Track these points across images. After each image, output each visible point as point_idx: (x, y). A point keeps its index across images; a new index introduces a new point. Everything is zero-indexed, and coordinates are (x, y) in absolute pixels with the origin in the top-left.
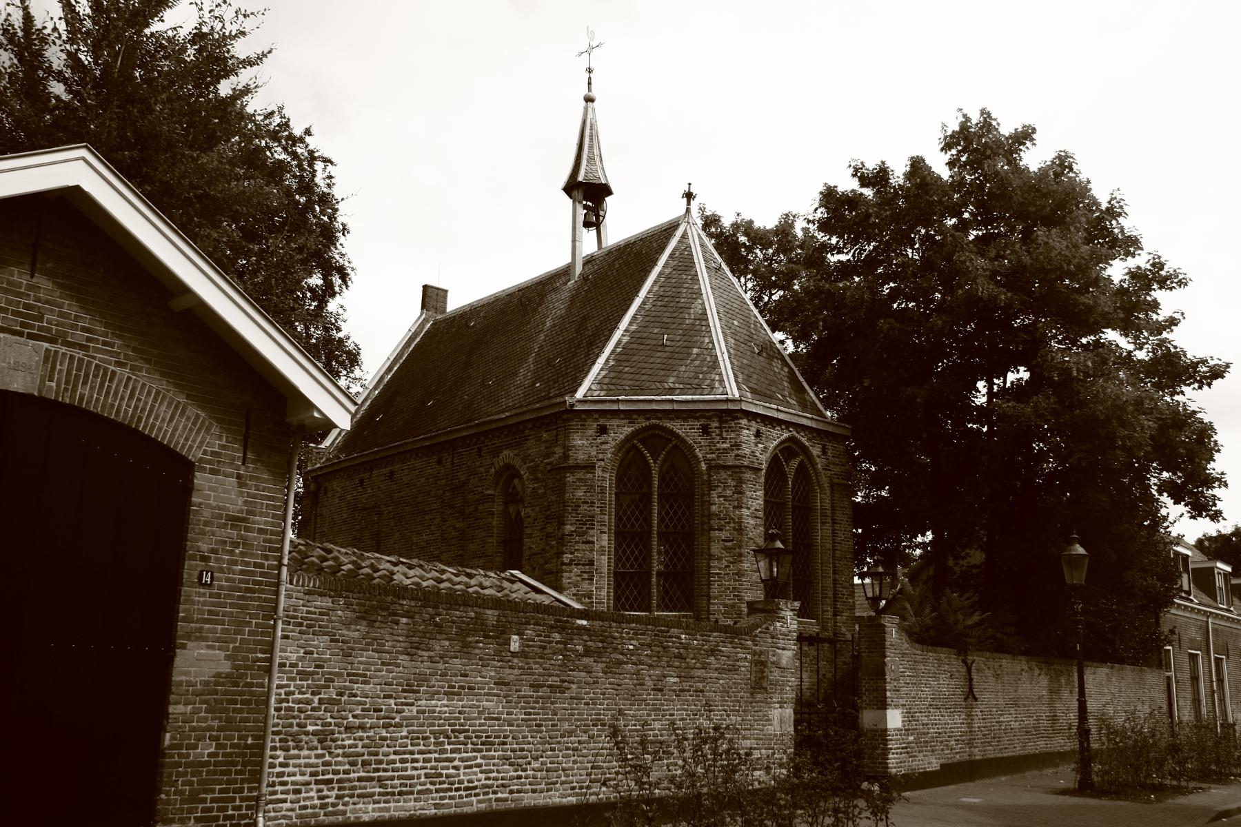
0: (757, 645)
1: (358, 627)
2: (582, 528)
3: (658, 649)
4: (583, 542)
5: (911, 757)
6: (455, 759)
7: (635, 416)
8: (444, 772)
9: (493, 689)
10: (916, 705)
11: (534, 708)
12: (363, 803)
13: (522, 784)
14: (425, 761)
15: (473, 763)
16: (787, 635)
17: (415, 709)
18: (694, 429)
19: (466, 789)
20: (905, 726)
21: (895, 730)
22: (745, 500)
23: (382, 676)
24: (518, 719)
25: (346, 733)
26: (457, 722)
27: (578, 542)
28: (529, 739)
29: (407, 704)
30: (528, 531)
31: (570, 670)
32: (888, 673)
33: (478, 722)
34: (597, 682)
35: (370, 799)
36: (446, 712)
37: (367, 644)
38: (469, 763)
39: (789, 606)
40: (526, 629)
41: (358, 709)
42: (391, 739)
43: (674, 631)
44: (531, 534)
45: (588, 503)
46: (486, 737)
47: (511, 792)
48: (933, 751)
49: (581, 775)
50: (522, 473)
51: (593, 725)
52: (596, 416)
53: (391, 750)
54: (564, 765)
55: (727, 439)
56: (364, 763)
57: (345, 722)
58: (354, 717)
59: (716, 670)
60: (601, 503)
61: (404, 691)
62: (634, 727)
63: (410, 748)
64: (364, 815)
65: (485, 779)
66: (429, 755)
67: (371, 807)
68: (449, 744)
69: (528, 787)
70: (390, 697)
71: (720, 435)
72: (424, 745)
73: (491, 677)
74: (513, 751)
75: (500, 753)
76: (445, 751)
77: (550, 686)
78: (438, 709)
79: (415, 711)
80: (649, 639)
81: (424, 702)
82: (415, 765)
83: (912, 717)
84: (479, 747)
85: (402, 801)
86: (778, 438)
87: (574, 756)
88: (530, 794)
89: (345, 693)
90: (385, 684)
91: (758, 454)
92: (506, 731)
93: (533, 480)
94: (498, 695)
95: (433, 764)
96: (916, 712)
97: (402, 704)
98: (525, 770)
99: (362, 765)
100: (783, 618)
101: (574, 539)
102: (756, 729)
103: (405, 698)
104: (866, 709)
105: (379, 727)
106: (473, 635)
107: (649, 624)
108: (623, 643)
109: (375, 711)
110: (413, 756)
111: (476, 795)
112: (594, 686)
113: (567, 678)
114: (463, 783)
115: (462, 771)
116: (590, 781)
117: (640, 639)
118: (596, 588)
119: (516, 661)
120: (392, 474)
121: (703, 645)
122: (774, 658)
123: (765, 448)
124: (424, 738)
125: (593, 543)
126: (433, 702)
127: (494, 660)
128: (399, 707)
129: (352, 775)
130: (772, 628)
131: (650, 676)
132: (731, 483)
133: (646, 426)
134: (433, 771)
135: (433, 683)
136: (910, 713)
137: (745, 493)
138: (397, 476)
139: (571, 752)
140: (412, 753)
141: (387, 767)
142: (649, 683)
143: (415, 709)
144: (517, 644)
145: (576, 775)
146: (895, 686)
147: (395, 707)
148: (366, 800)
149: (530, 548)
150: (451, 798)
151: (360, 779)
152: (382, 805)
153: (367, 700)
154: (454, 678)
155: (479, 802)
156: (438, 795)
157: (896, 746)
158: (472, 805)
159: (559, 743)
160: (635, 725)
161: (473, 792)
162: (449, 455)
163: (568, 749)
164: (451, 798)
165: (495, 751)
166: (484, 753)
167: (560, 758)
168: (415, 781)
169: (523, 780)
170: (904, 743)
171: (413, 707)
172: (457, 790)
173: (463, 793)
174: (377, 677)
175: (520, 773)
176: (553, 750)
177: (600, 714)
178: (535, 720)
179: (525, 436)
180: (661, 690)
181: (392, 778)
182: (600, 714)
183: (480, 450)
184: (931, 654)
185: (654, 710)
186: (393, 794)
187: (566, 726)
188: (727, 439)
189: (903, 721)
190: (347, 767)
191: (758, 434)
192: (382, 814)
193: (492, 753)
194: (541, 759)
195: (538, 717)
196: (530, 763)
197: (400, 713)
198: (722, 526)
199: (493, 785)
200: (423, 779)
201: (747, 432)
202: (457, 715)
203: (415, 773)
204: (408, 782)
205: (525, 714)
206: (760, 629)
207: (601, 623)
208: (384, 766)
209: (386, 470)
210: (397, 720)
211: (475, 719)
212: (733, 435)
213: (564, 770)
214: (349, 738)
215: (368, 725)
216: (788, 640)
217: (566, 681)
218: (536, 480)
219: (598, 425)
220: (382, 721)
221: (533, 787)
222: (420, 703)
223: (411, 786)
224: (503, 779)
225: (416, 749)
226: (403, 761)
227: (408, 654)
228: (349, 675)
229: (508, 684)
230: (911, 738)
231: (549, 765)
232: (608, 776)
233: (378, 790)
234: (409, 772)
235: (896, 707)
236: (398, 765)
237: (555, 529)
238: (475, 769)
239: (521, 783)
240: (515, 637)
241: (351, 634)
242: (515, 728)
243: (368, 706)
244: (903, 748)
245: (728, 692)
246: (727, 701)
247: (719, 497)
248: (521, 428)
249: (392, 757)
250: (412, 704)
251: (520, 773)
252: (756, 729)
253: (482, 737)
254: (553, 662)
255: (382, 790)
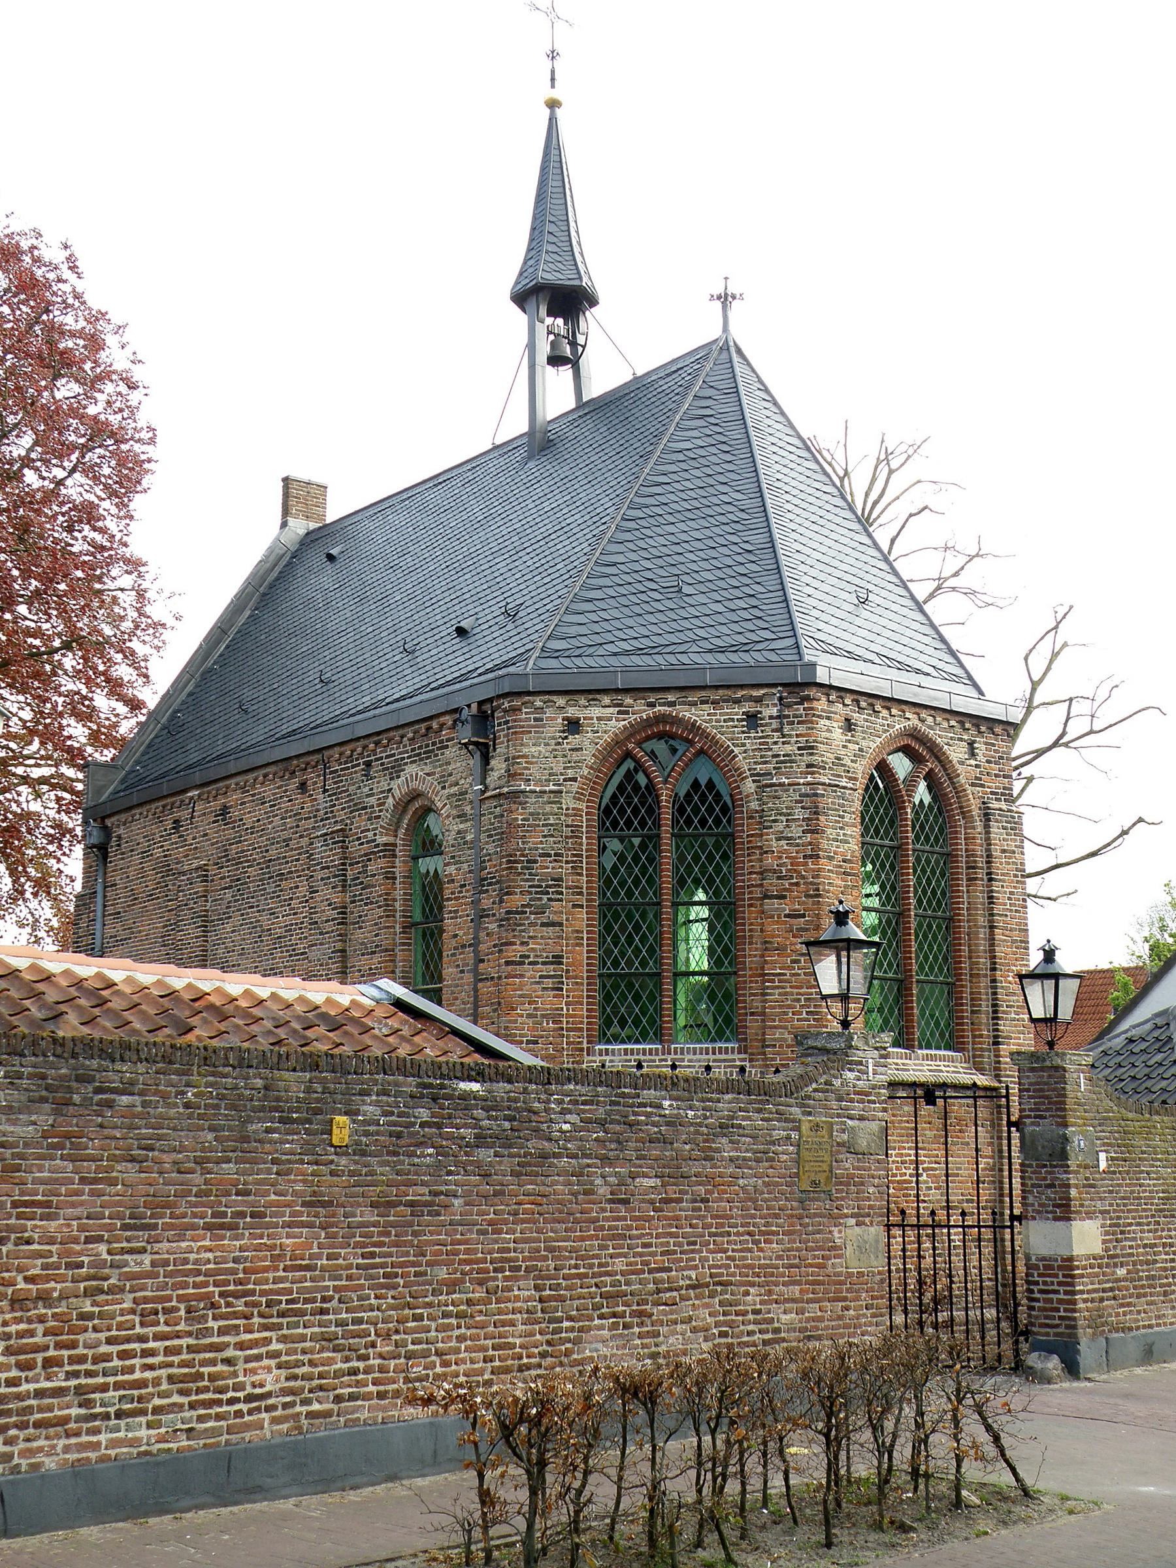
0: (810, 1114)
1: (34, 1118)
2: (540, 899)
3: (618, 1128)
4: (543, 925)
5: (1122, 1305)
6: (227, 1345)
7: (629, 701)
8: (205, 1370)
9: (301, 1214)
10: (1129, 1211)
11: (380, 1244)
12: (47, 1438)
13: (358, 1384)
14: (168, 1351)
15: (263, 1350)
16: (868, 1094)
17: (147, 1259)
18: (733, 720)
19: (249, 1399)
20: (1107, 1250)
21: (1088, 1257)
22: (824, 844)
23: (82, 1204)
24: (350, 1267)
25: (13, 1310)
26: (231, 1278)
27: (535, 924)
28: (373, 1301)
29: (131, 1251)
30: (450, 905)
31: (449, 1173)
32: (1072, 1155)
33: (271, 1275)
34: (502, 1193)
35: (59, 1429)
36: (208, 1261)
37: (52, 1147)
38: (255, 1351)
39: (872, 1042)
40: (364, 1103)
41: (35, 1267)
42: (101, 1316)
43: (649, 1094)
44: (456, 912)
45: (549, 855)
46: (288, 1302)
47: (338, 1399)
48: (1165, 1294)
49: (472, 1362)
50: (439, 805)
51: (495, 1270)
52: (561, 701)
53: (102, 1336)
54: (440, 1345)
55: (790, 736)
56: (48, 1363)
57: (10, 1290)
58: (27, 1280)
59: (731, 1160)
60: (574, 855)
61: (125, 1227)
62: (573, 1271)
63: (138, 1330)
64: (46, 1460)
65: (287, 1379)
66: (176, 1342)
67: (62, 1443)
68: (214, 1319)
69: (371, 1388)
70: (99, 1239)
71: (780, 730)
72: (167, 1323)
73: (295, 1193)
74: (340, 1323)
75: (316, 1329)
76: (208, 1332)
77: (411, 1204)
78: (192, 1256)
79: (147, 1262)
80: (601, 1110)
81: (165, 1245)
82: (150, 1360)
83: (1122, 1232)
84: (275, 1320)
85: (123, 1428)
86: (885, 731)
87: (459, 1327)
88: (375, 1401)
89: (9, 1238)
90: (87, 1218)
91: (847, 761)
92: (327, 1288)
93: (459, 817)
94: (310, 1225)
95: (184, 1357)
96: (1130, 1225)
97: (123, 1251)
98: (365, 1358)
99: (44, 1367)
100: (861, 1063)
101: (528, 918)
102: (811, 1266)
103: (128, 1241)
104: (1034, 1218)
105: (77, 1297)
106: (260, 1120)
107: (601, 1084)
108: (551, 1121)
109: (69, 1266)
110: (144, 1346)
111: (268, 1409)
112: (496, 1200)
113: (443, 1188)
114: (244, 1389)
115: (241, 1367)
116: (492, 1373)
117: (584, 1111)
118: (567, 1004)
119: (343, 1161)
120: (225, 810)
121: (706, 1118)
122: (845, 1137)
123: (861, 750)
124: (166, 1311)
125: (561, 924)
126: (184, 1245)
127: (302, 1162)
128: (117, 1257)
129: (25, 1387)
130: (837, 1083)
131: (603, 1177)
132: (799, 814)
133: (649, 718)
134: (186, 1370)
135: (182, 1210)
136: (1118, 1225)
137: (823, 832)
138: (235, 813)
139: (454, 1321)
140: (142, 1339)
141: (93, 1368)
142: (604, 1191)
143: (147, 1259)
144: (346, 1132)
145: (464, 1361)
146: (1087, 1179)
147: (109, 1258)
148: (52, 1431)
149: (456, 936)
150: (219, 1417)
151: (39, 1394)
152: (85, 1439)
153: (54, 1248)
154: (223, 1200)
155: (274, 1421)
156: (194, 1413)
157: (1090, 1287)
158: (262, 1428)
159: (430, 1305)
160: (576, 1267)
161: (263, 1404)
162: (319, 776)
163: (446, 1315)
164: (219, 1417)
165: (305, 1327)
166: (285, 1332)
167: (433, 1334)
168: (150, 1389)
169: (361, 1377)
170: (1108, 1281)
171: (144, 1256)
172: (231, 1402)
173: (244, 1407)
174: (73, 1205)
175: (355, 1364)
176: (418, 1318)
177: (508, 1250)
178: (383, 1266)
179: (441, 742)
180: (625, 1202)
181: (104, 1388)
182: (508, 1250)
183: (368, 764)
184: (1156, 1118)
185: (613, 1237)
186: (107, 1416)
187: (442, 1273)
188: (790, 736)
189: (1104, 1242)
190: (14, 1373)
191: (849, 725)
192: (84, 1455)
193: (300, 1331)
194: (394, 1337)
195: (389, 1260)
196: (373, 1345)
197: (119, 1267)
198: (786, 890)
199: (303, 1389)
200: (164, 1386)
201: (827, 722)
202: (231, 1265)
203: (148, 1375)
204: (136, 1393)
205: (363, 1256)
206: (814, 1086)
207: (508, 1087)
208: (88, 1366)
209: (215, 805)
210: (112, 1281)
211: (266, 1270)
212: (802, 729)
213: (438, 1353)
214: (18, 1321)
215: (55, 1295)
216: (869, 1101)
217: (442, 1193)
218: (462, 816)
219: (563, 720)
220: (82, 1285)
221: (381, 1388)
222: (157, 1246)
223: (140, 1399)
224: (321, 1377)
225: (150, 1331)
226: (123, 1355)
227: (133, 1160)
228: (15, 1205)
229: (330, 1204)
230: (1121, 1272)
231: (411, 1347)
232: (525, 1360)
233: (74, 1411)
234: (137, 1375)
235: (1090, 1215)
236: (116, 1363)
237: (494, 903)
238: (266, 1362)
239: (358, 1381)
240: (341, 1119)
241: (18, 1129)
242: (344, 1283)
243: (54, 1259)
244: (1104, 1291)
245: (755, 1201)
246: (753, 1217)
247: (778, 839)
248: (435, 725)
249: (104, 1349)
250: (143, 1251)
251: (355, 1364)
252: (811, 1266)
253: (281, 1302)
254: (416, 1160)
255: (83, 1411)
